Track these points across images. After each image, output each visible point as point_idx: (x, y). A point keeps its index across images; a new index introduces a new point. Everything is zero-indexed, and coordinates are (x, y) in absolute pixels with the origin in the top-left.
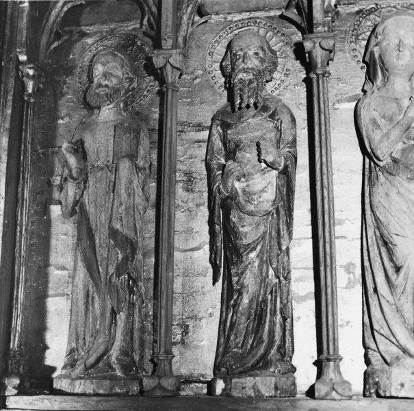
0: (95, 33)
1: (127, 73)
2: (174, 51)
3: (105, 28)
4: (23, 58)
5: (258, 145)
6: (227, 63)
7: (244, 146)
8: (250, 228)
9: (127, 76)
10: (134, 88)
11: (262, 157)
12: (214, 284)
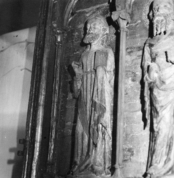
0: (90, 11)
1: (103, 27)
2: (122, 11)
3: (95, 7)
4: (55, 25)
5: (166, 52)
6: (151, 14)
7: (160, 54)
8: (163, 98)
9: (103, 28)
10: (107, 34)
11: (169, 59)
12: (144, 129)
